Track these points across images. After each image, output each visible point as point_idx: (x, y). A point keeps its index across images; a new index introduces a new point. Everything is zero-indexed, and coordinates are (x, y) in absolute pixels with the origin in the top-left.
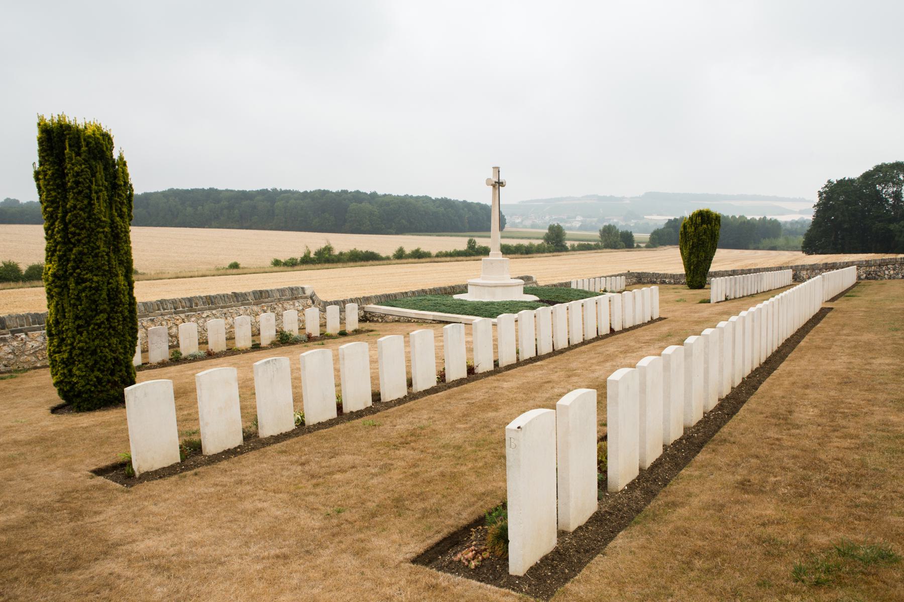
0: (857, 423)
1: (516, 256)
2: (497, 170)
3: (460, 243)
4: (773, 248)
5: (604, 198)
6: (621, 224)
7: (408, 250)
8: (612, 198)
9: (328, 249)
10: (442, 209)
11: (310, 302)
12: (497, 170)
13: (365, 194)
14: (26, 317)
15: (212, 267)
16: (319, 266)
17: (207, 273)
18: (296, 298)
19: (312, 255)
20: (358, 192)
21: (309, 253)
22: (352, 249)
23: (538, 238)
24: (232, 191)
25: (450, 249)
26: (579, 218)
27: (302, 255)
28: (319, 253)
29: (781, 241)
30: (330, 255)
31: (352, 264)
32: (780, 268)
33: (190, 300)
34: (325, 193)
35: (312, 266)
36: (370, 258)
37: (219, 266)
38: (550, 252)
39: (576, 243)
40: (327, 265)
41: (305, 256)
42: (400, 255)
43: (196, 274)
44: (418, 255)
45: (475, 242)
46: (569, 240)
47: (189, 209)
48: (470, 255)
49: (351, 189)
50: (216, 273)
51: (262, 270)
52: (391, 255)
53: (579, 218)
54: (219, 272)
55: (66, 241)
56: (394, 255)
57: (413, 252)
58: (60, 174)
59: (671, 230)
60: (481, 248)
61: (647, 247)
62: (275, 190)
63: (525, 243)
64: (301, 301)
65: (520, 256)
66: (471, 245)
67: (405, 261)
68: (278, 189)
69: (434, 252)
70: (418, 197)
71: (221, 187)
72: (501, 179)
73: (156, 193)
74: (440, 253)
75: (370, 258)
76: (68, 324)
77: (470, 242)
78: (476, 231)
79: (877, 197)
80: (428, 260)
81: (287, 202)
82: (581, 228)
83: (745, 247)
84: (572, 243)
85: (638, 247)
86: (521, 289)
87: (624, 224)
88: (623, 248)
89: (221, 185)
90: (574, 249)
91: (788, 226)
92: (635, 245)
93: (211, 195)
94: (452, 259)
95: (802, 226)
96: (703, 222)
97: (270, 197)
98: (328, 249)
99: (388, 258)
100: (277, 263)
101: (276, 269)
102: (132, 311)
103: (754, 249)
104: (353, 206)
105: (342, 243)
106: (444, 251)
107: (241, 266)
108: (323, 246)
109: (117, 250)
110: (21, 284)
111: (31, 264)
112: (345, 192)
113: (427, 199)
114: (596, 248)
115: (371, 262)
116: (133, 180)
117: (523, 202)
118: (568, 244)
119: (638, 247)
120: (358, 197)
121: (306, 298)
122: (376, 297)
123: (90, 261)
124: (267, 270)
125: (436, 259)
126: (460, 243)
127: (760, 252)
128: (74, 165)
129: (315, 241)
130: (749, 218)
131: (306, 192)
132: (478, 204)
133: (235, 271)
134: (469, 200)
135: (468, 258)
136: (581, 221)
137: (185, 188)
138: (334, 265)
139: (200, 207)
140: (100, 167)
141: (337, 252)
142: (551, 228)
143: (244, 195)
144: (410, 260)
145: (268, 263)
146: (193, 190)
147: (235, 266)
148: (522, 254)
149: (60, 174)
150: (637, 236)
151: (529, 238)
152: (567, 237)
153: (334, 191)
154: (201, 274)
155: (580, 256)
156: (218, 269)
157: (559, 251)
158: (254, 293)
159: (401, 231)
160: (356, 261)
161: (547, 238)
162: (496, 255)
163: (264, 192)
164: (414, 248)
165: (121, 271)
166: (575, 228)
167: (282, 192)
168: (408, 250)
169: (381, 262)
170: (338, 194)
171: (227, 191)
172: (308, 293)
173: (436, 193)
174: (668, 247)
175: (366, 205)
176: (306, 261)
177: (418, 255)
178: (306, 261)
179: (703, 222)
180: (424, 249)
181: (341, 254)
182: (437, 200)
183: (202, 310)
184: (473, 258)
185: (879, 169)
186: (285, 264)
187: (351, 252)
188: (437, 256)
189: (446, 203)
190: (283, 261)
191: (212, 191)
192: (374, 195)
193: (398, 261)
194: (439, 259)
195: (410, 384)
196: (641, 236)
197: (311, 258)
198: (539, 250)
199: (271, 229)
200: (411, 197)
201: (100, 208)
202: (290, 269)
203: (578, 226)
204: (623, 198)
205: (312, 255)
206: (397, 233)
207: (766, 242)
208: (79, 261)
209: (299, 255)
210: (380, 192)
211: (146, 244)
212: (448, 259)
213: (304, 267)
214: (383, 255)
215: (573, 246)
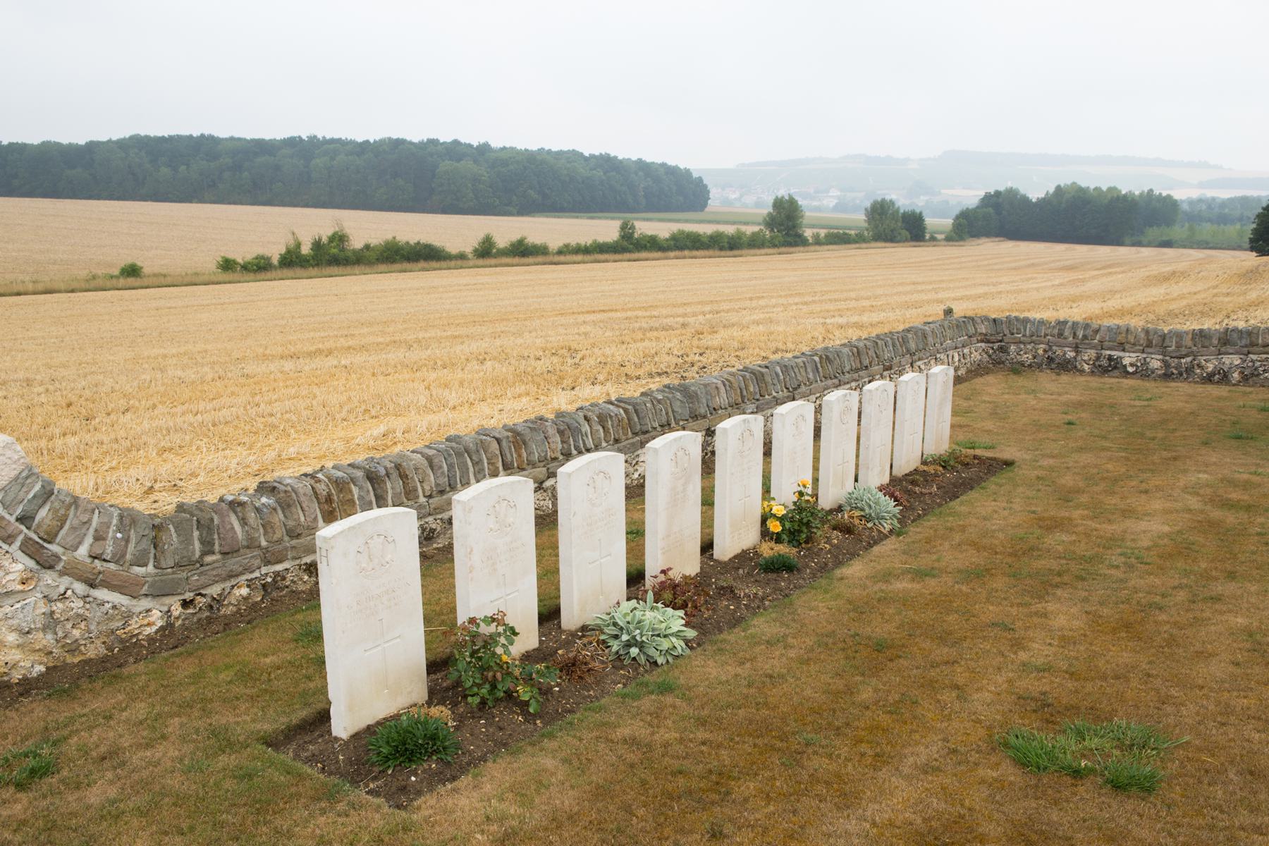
1: (711, 252)
3: (607, 229)
4: (1167, 244)
6: (904, 202)
7: (502, 242)
9: (339, 239)
10: (599, 173)
13: (470, 146)
20: (456, 143)
21: (299, 245)
22: (389, 237)
23: (754, 223)
24: (239, 139)
29: (1178, 232)
30: (343, 250)
31: (382, 267)
34: (399, 143)
35: (299, 271)
36: (425, 255)
38: (775, 246)
41: (289, 251)
42: (486, 251)
43: (30, 287)
44: (522, 251)
45: (633, 227)
46: (813, 226)
47: (165, 171)
49: (445, 137)
52: (468, 250)
53: (835, 193)
56: (476, 251)
57: (512, 245)
59: (991, 210)
61: (949, 239)
62: (313, 139)
63: (730, 230)
65: (717, 253)
67: (493, 261)
68: (320, 136)
69: (554, 245)
70: (560, 153)
71: (222, 133)
74: (567, 246)
75: (425, 255)
77: (623, 227)
78: (659, 210)
80: (540, 259)
81: (333, 159)
82: (836, 208)
83: (1118, 242)
84: (815, 231)
85: (933, 239)
87: (907, 202)
88: (906, 240)
89: (222, 130)
90: (818, 242)
91: (1185, 207)
92: (927, 236)
93: (204, 146)
94: (588, 258)
95: (1209, 207)
98: (339, 239)
99: (462, 256)
100: (227, 265)
101: (228, 276)
103: (1133, 245)
104: (445, 165)
107: (146, 270)
112: (433, 142)
113: (575, 156)
115: (422, 264)
116: (1030, 196)
118: (808, 233)
119: (933, 239)
120: (455, 150)
125: (557, 259)
126: (607, 229)
127: (1146, 252)
129: (311, 224)
130: (1164, 194)
132: (663, 165)
133: (131, 281)
134: (649, 159)
135: (617, 257)
137: (160, 134)
138: (349, 269)
139: (183, 167)
142: (778, 204)
143: (261, 147)
146: (171, 138)
147: (132, 271)
148: (721, 249)
150: (930, 221)
151: (718, 222)
152: (805, 222)
153: (416, 140)
154: (40, 287)
155: (828, 254)
157: (790, 245)
159: (527, 208)
160: (394, 262)
161: (771, 222)
163: (293, 143)
164: (515, 237)
166: (822, 205)
167: (327, 142)
168: (502, 242)
169: (444, 264)
170: (423, 146)
171: (232, 139)
173: (590, 147)
174: (984, 240)
176: (293, 261)
177: (522, 251)
178: (293, 261)
180: (534, 239)
181: (367, 247)
182: (592, 156)
184: (627, 256)
186: (245, 268)
188: (560, 252)
189: (607, 162)
190: (240, 261)
192: (484, 149)
193: (481, 262)
194: (562, 258)
195: (707, 547)
196: (937, 222)
198: (755, 243)
199: (307, 206)
200: (549, 152)
202: (252, 276)
203: (832, 205)
205: (306, 250)
206: (521, 213)
207: (1152, 232)
209: (275, 252)
210: (496, 144)
212: (579, 257)
213: (287, 272)
215: (816, 237)
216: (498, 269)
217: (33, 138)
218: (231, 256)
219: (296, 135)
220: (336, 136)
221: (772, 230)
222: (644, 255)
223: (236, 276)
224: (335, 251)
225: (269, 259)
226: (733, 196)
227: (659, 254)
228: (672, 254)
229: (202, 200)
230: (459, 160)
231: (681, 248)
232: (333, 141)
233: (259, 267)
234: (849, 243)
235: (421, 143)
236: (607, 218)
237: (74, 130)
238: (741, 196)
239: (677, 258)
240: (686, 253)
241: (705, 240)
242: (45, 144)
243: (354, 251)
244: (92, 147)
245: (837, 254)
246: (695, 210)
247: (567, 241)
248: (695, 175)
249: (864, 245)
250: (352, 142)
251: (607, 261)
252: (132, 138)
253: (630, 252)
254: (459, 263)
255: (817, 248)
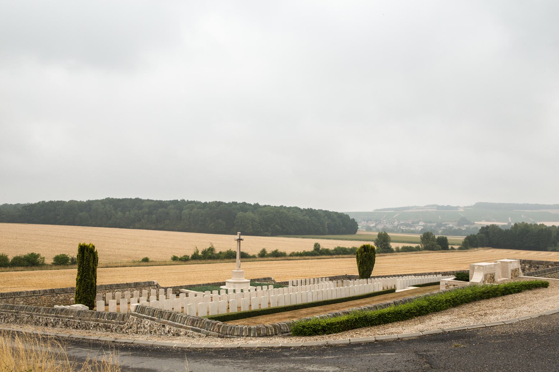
1: (350, 256)
5: (443, 207)
8: (448, 207)
9: (211, 249)
11: (156, 287)
13: (250, 205)
14: (60, 289)
15: (131, 260)
16: (203, 261)
17: (128, 264)
19: (200, 254)
20: (244, 203)
21: (198, 252)
25: (300, 250)
26: (421, 223)
27: (193, 253)
30: (212, 254)
31: (227, 260)
32: (378, 277)
33: (111, 285)
34: (219, 204)
35: (199, 261)
37: (135, 260)
39: (401, 246)
40: (209, 261)
41: (195, 254)
47: (120, 213)
48: (316, 255)
50: (132, 264)
51: (164, 263)
53: (421, 223)
54: (135, 264)
55: (83, 272)
56: (259, 254)
58: (83, 256)
60: (323, 249)
66: (317, 246)
67: (266, 259)
69: (288, 252)
71: (144, 197)
73: (97, 201)
74: (293, 253)
76: (81, 291)
80: (283, 258)
88: (439, 249)
90: (398, 251)
92: (450, 247)
96: (365, 251)
97: (179, 205)
98: (211, 249)
99: (254, 257)
100: (175, 258)
102: (96, 289)
105: (223, 242)
106: (296, 251)
107: (150, 260)
108: (208, 247)
109: (94, 274)
110: (8, 269)
111: (14, 256)
112: (235, 203)
114: (417, 249)
117: (377, 210)
118: (393, 245)
120: (244, 207)
122: (185, 286)
123: (87, 276)
124: (167, 263)
125: (289, 258)
128: (86, 254)
131: (206, 203)
136: (424, 226)
138: (215, 261)
139: (128, 212)
140: (92, 255)
141: (218, 252)
142: (380, 236)
144: (270, 258)
145: (169, 258)
147: (146, 260)
149: (83, 256)
154: (122, 264)
156: (134, 262)
157: (385, 252)
158: (134, 283)
160: (230, 258)
163: (175, 202)
165: (94, 279)
167: (189, 202)
169: (248, 260)
172: (155, 284)
174: (480, 248)
175: (249, 214)
176: (195, 258)
177: (276, 255)
178: (195, 258)
179: (365, 251)
180: (281, 250)
181: (220, 253)
182: (304, 210)
183: (115, 289)
184: (317, 257)
186: (181, 259)
187: (228, 251)
188: (291, 255)
189: (310, 212)
191: (138, 201)
192: (257, 206)
193: (261, 259)
194: (291, 258)
197: (198, 256)
201: (91, 264)
202: (183, 263)
204: (458, 207)
205: (200, 254)
206: (272, 235)
208: (85, 276)
209: (190, 254)
210: (262, 204)
211: (100, 272)
212: (298, 258)
213: (194, 261)
214: (251, 254)
216: (268, 262)
217: (67, 199)
218: (176, 255)
219: (176, 199)
220: (193, 200)
221: (378, 246)
222: (323, 257)
223: (177, 263)
224: (210, 254)
225: (188, 256)
226: (372, 225)
227: (329, 256)
228: (335, 256)
229: (134, 228)
230: (246, 212)
231: (338, 254)
232: (191, 202)
233: (185, 260)
234: (412, 251)
235: (229, 203)
236: (310, 238)
237: (83, 196)
238: (376, 225)
239: (336, 258)
240: (340, 256)
241: (349, 251)
242: (71, 202)
243: (216, 254)
244: (90, 204)
245: (404, 256)
246: (352, 234)
247: (293, 251)
248: (351, 218)
249: (419, 252)
250: (199, 203)
251: (309, 259)
252: (107, 199)
253: (318, 255)
254: (254, 259)
255: (398, 254)
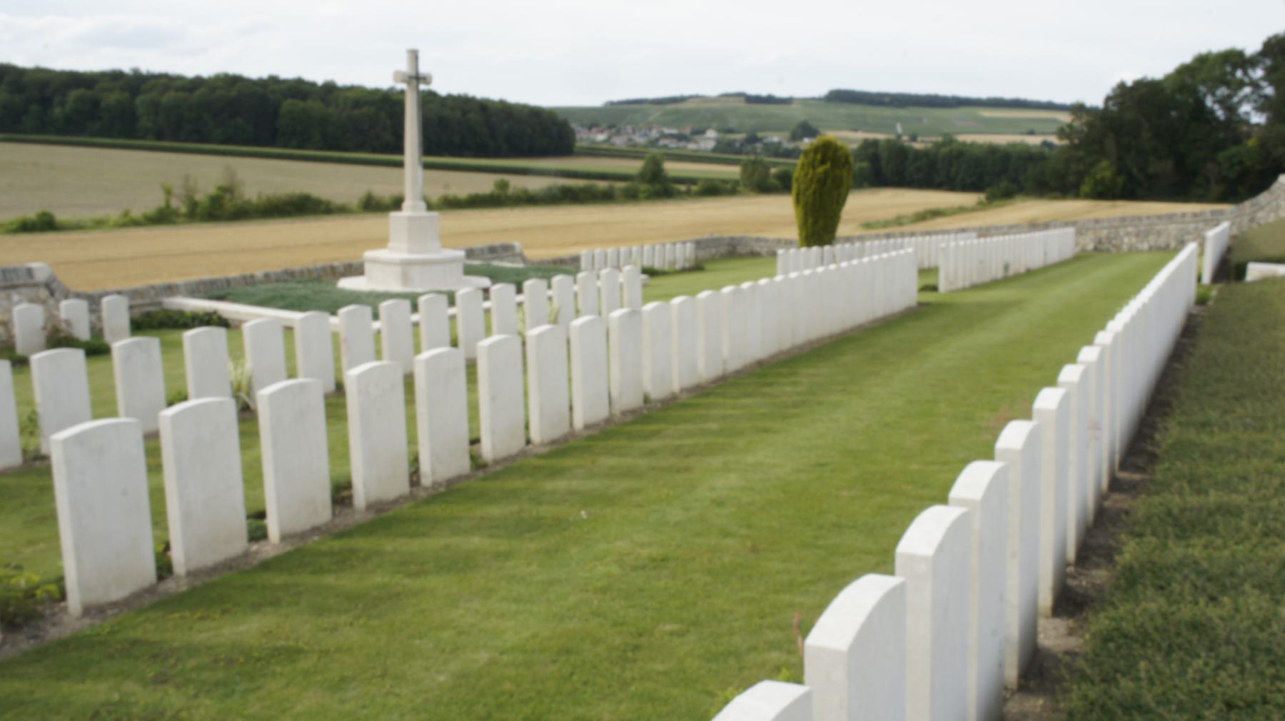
0: (712, 489)
2: (414, 56)
12: (414, 56)
13: (313, 85)
18: (14, 287)
26: (711, 134)
28: (216, 201)
34: (235, 81)
64: (24, 290)
72: (423, 70)
75: (302, 207)
79: (1200, 112)
86: (459, 268)
112: (274, 80)
120: (299, 89)
121: (36, 285)
162: (412, 208)
163: (116, 77)
171: (38, 71)
175: (314, 105)
185: (1202, 60)
192: (330, 88)
214: (338, 200)
